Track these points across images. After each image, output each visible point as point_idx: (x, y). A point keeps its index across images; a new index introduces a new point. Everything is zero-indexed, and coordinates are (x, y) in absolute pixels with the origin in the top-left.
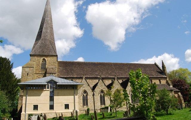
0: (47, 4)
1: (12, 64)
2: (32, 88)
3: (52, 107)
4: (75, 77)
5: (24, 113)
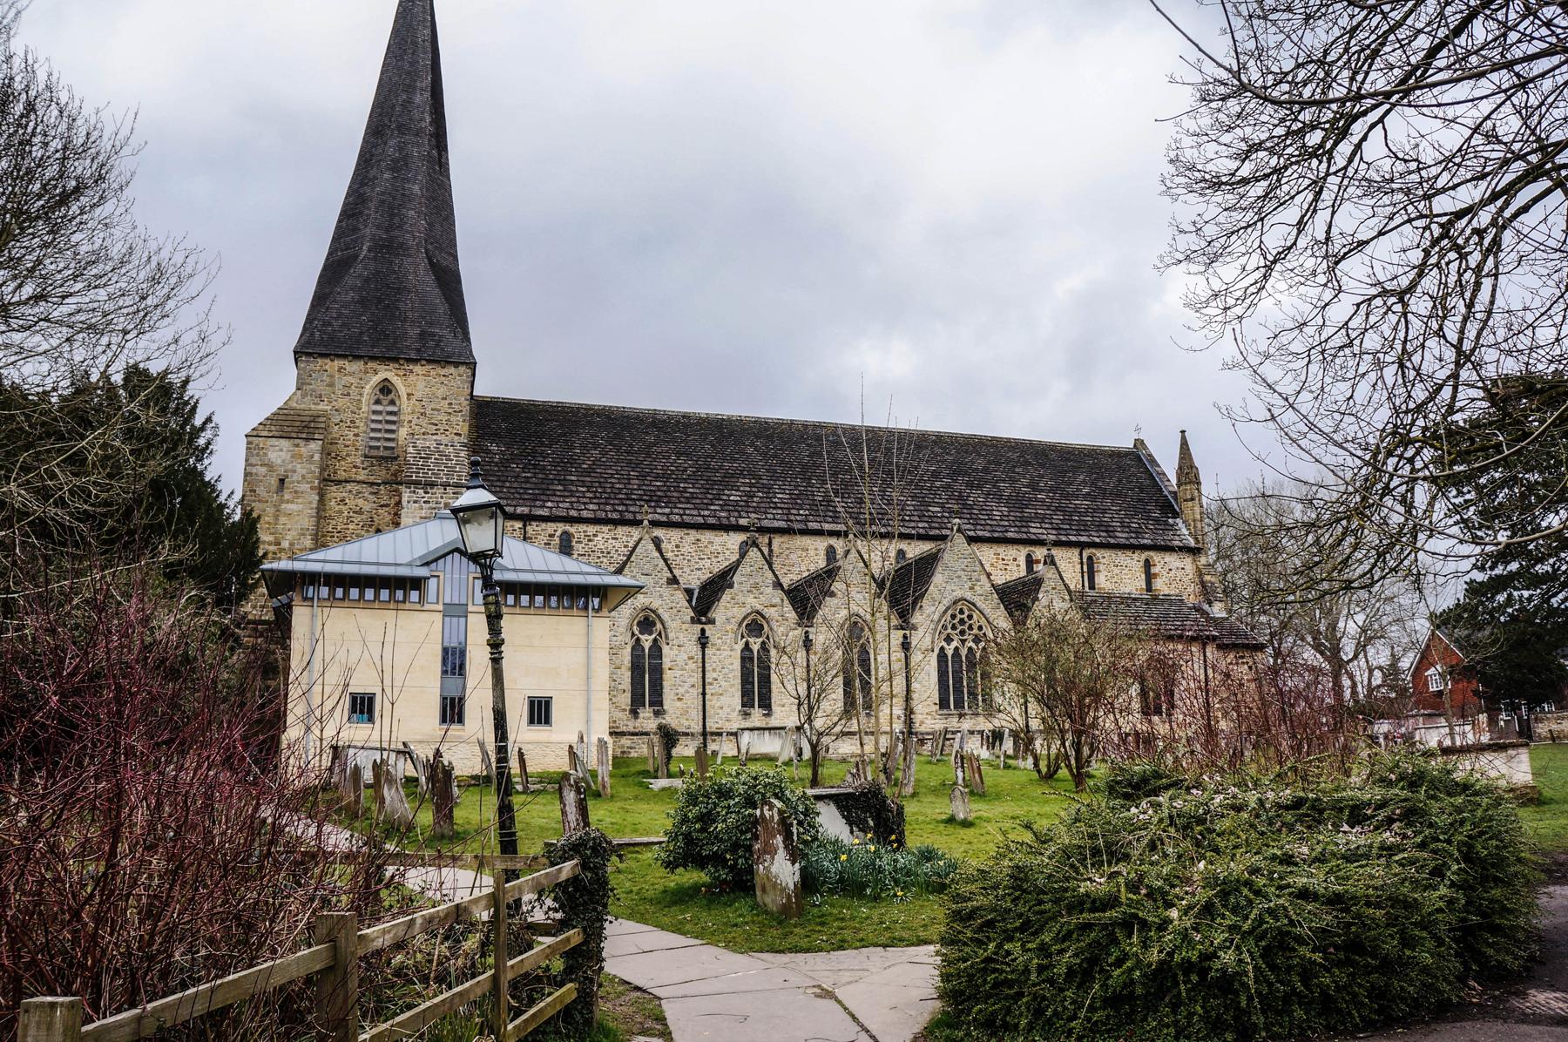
2: (339, 592)
4: (585, 514)
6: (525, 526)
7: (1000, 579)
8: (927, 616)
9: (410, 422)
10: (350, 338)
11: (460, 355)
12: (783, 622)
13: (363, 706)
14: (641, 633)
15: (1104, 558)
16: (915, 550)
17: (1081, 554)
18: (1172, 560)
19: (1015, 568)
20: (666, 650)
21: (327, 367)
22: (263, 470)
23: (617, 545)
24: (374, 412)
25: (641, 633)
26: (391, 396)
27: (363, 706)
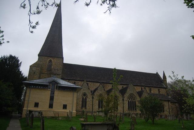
0: (61, 1)
1: (21, 63)
2: (35, 87)
3: (51, 106)
4: (78, 79)
5: (26, 109)
7: (137, 91)
8: (127, 95)
13: (37, 105)
15: (152, 89)
16: (125, 86)
18: (163, 90)
20: (87, 99)
27: (37, 105)
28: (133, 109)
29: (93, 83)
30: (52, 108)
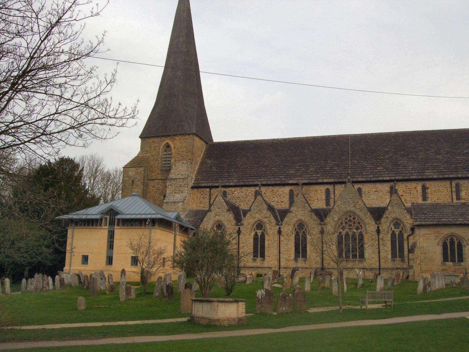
3: (110, 261)
4: (231, 184)
6: (210, 190)
9: (175, 156)
10: (8, 177)
11: (189, 131)
12: (312, 223)
14: (258, 230)
17: (451, 183)
19: (415, 192)
21: (149, 141)
22: (127, 178)
23: (243, 194)
24: (164, 155)
25: (395, 228)
26: (170, 148)
28: (354, 256)
29: (271, 188)
30: (112, 264)
